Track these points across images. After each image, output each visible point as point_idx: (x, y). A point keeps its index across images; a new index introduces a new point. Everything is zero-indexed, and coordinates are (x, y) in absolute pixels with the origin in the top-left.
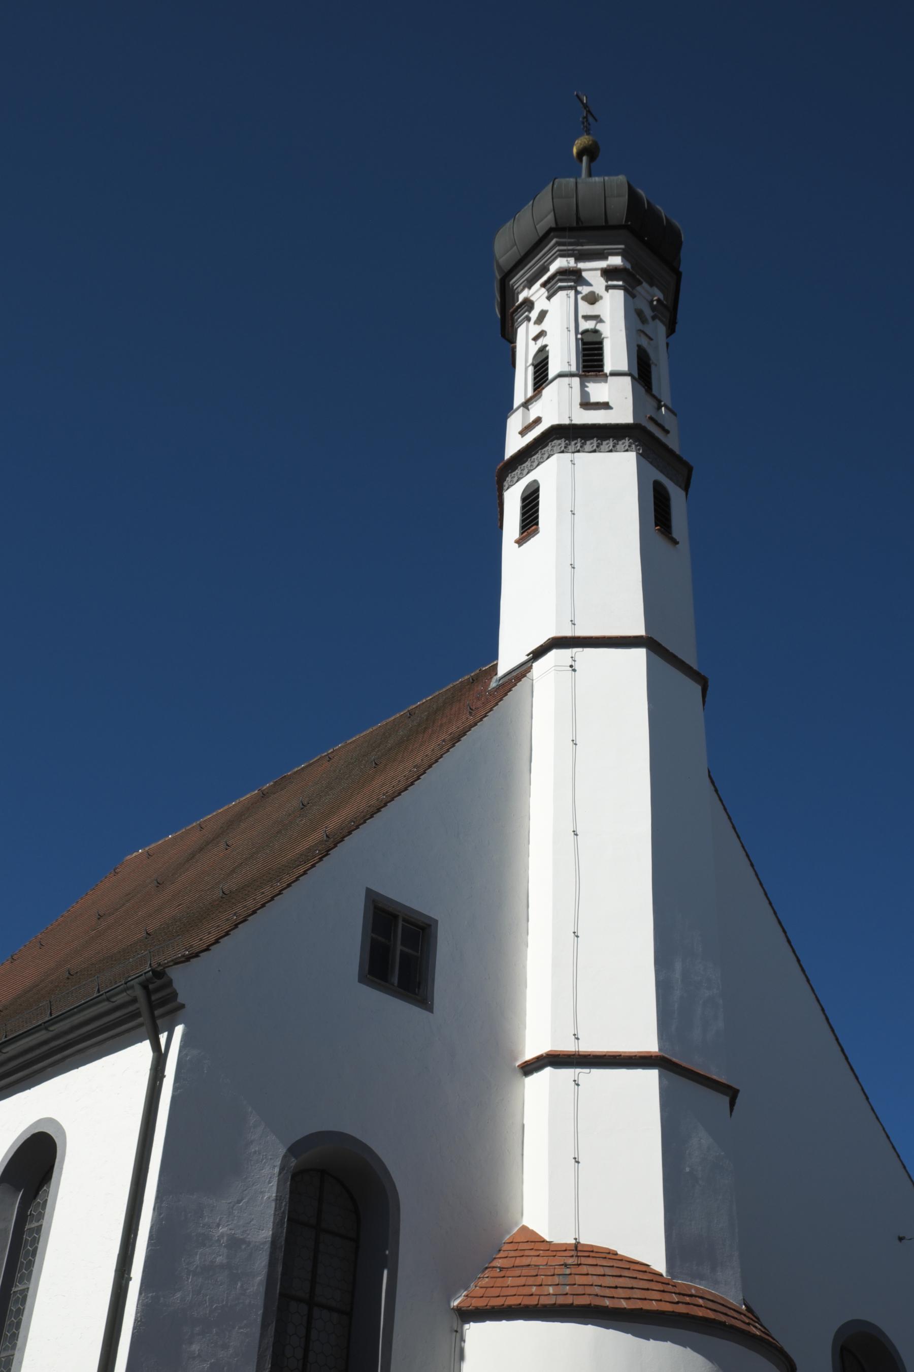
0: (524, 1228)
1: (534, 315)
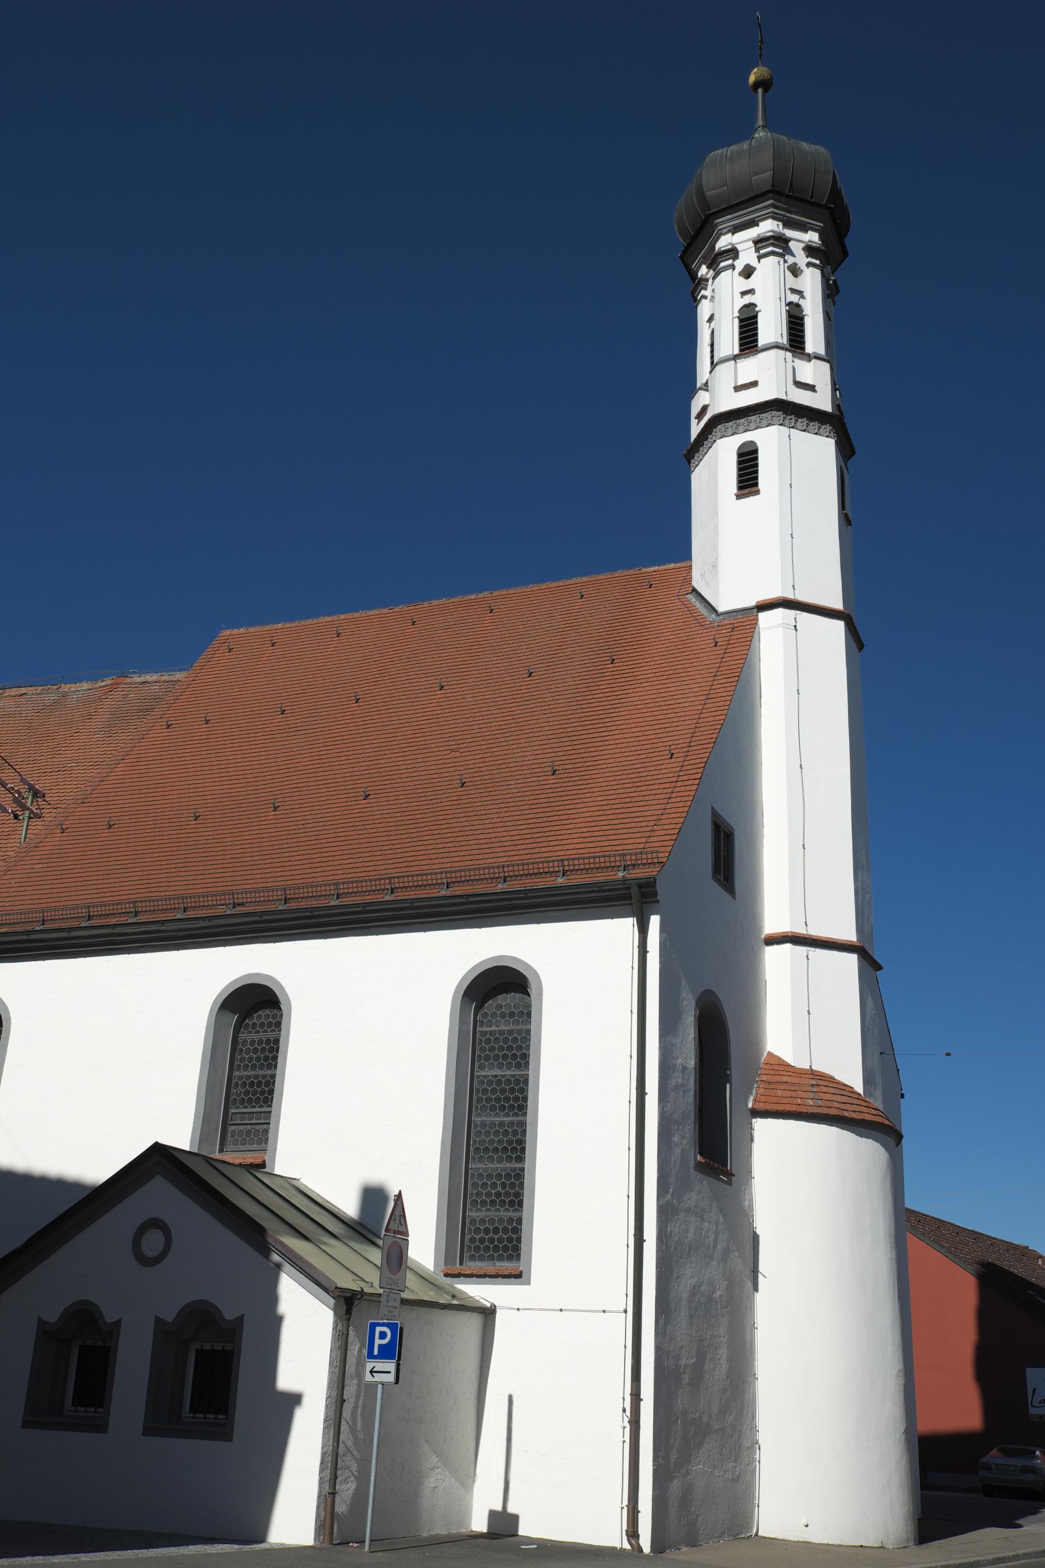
0: (770, 1053)
1: (740, 265)
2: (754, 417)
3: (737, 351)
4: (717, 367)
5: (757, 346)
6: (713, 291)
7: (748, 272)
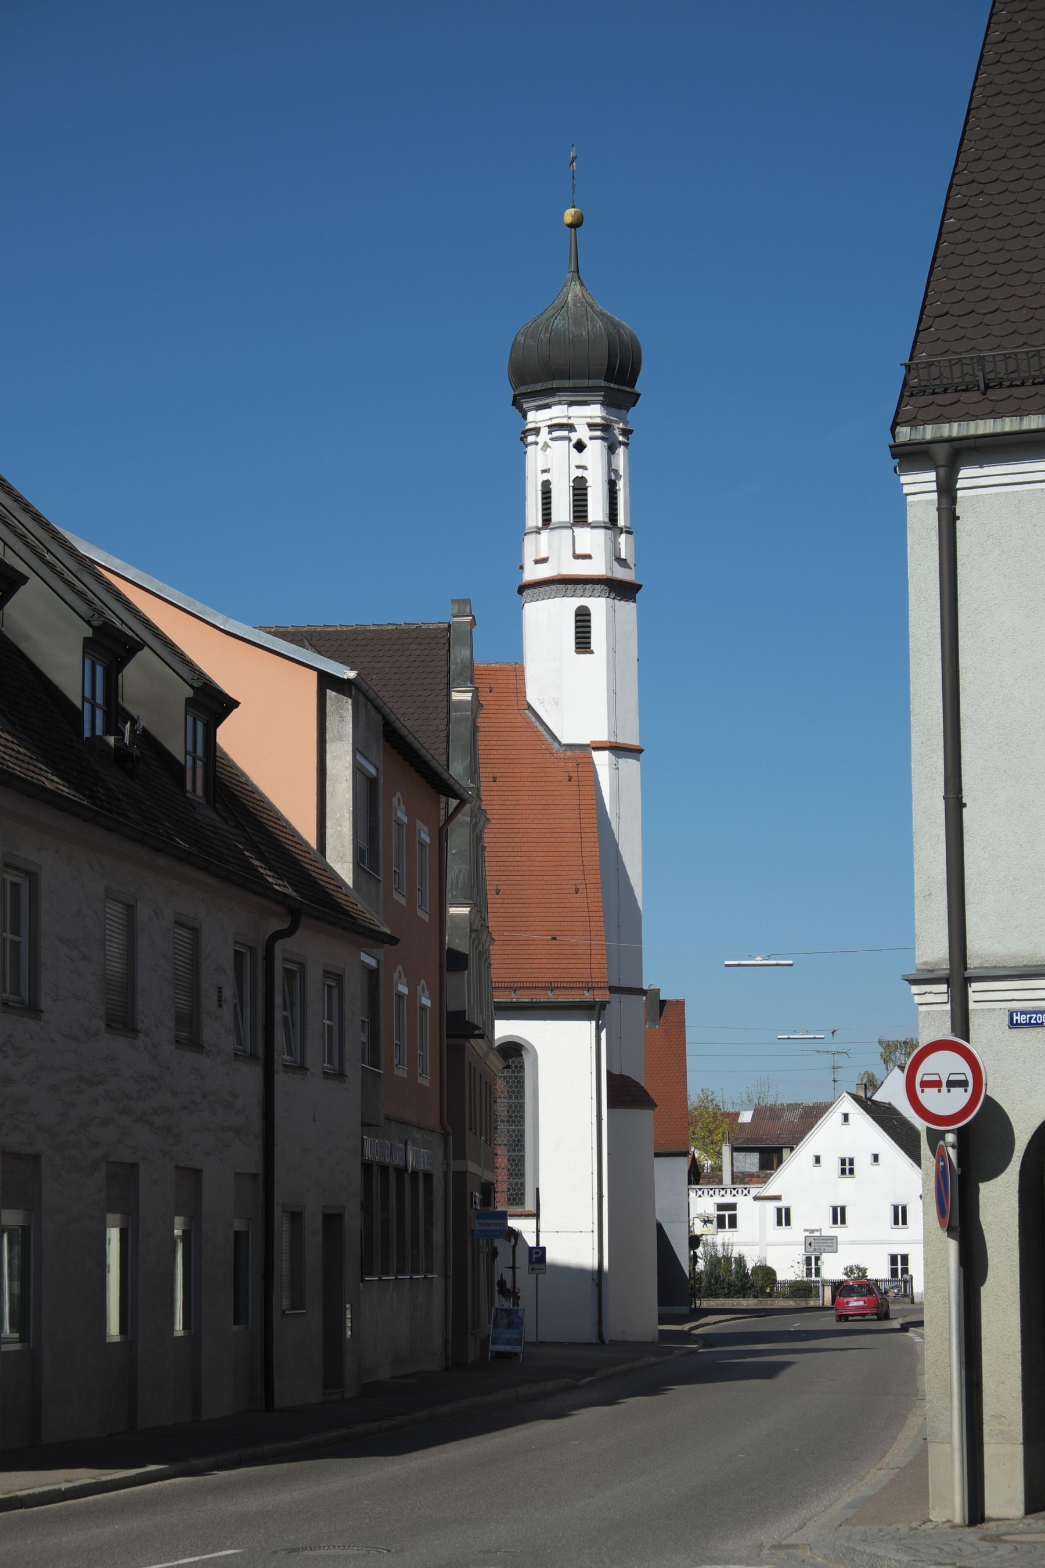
3: (540, 525)
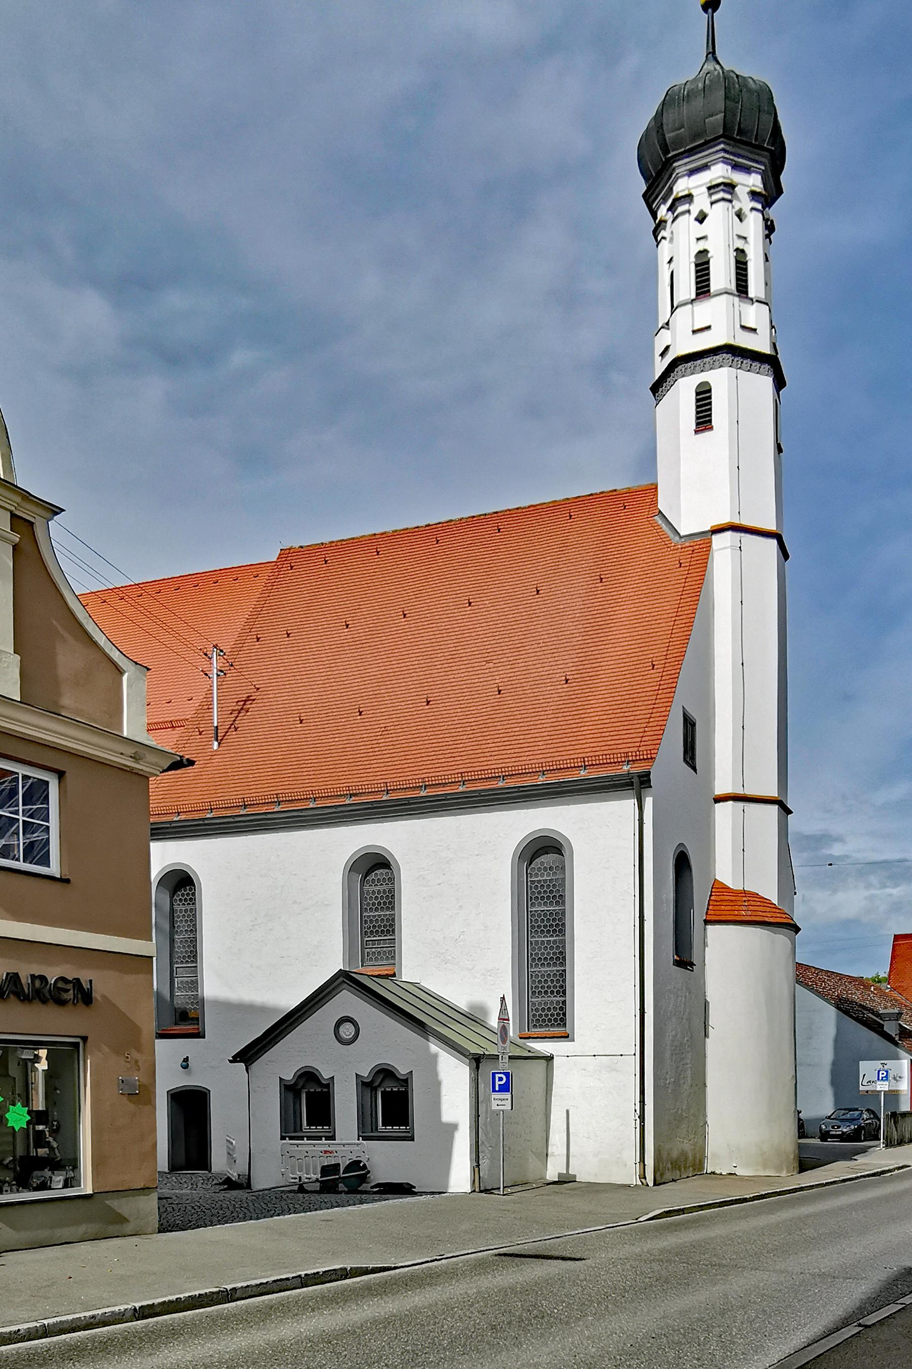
1: (695, 210)
2: (708, 359)
3: (693, 296)
4: (677, 310)
5: (709, 291)
6: (672, 233)
7: (701, 218)
